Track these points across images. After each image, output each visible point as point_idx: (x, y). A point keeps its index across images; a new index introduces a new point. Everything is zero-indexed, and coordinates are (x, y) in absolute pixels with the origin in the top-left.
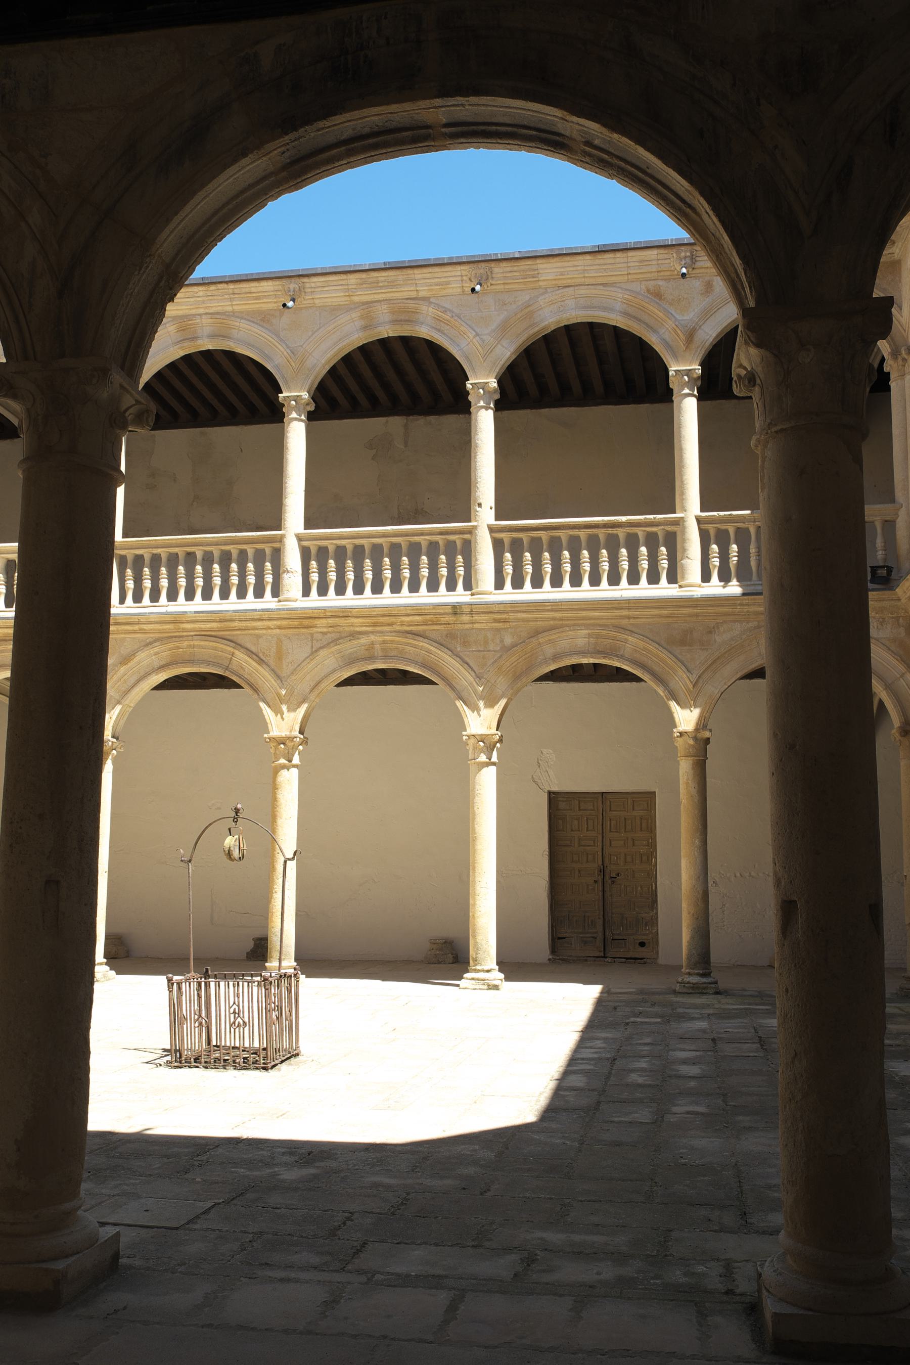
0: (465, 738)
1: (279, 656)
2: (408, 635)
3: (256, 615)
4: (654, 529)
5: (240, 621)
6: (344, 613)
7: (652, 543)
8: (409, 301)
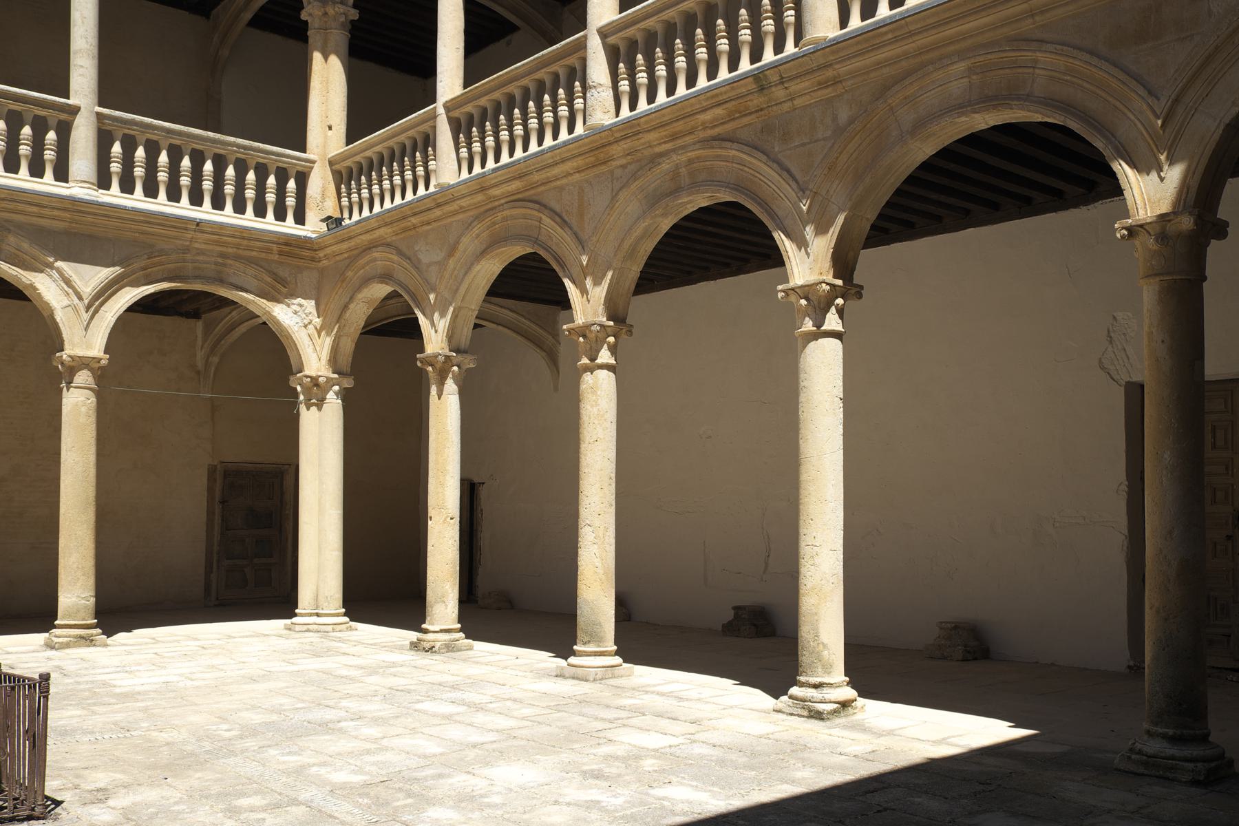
0: (780, 295)
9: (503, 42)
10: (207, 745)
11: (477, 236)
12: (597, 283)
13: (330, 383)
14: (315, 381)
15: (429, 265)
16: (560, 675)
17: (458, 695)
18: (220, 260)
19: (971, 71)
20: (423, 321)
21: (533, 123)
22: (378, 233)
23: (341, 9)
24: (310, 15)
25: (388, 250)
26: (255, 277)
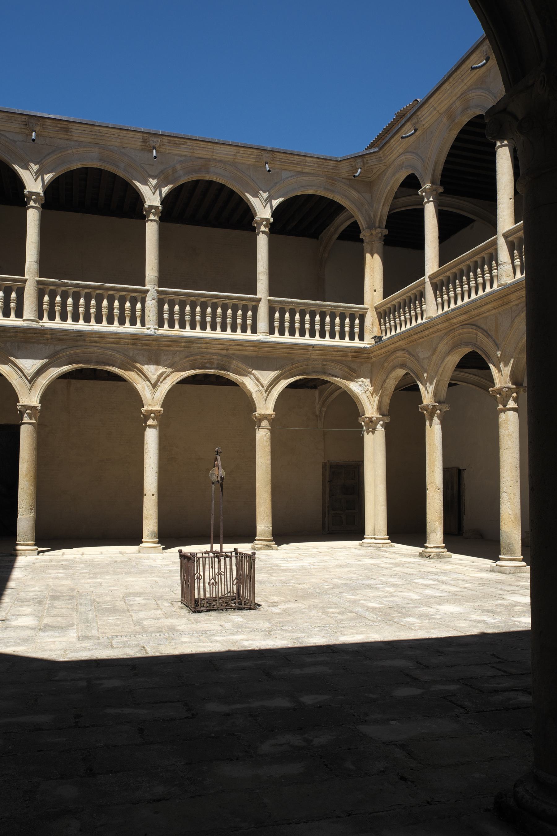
9: (469, 227)
10: (318, 591)
11: (447, 343)
12: (506, 365)
13: (378, 420)
14: (370, 419)
15: (423, 359)
16: (492, 570)
17: (437, 577)
18: (324, 363)
20: (421, 387)
21: (473, 283)
22: (398, 344)
23: (379, 230)
24: (364, 236)
25: (404, 352)
26: (341, 369)
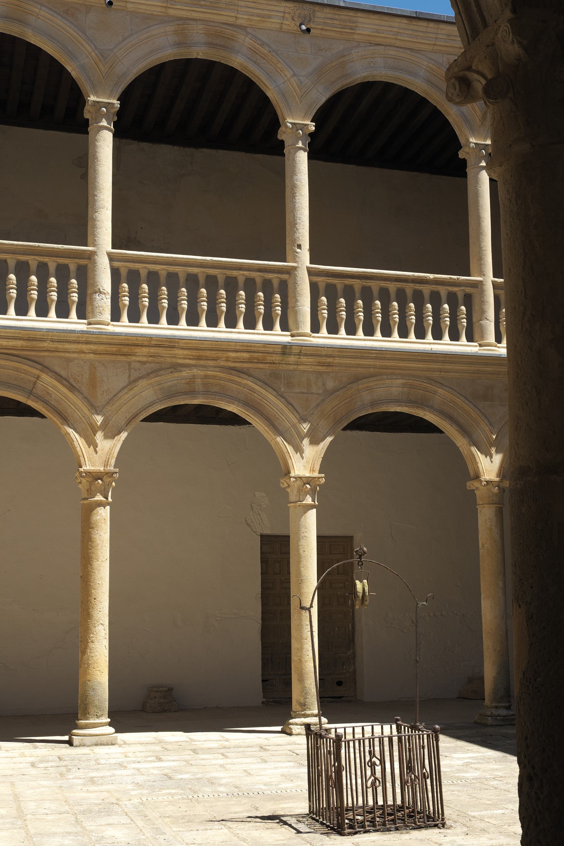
1: (93, 383)
2: (232, 372)
3: (72, 337)
4: (455, 289)
5: (53, 341)
6: (170, 343)
7: (63, 275)
8: (224, 26)
19: (404, 385)
